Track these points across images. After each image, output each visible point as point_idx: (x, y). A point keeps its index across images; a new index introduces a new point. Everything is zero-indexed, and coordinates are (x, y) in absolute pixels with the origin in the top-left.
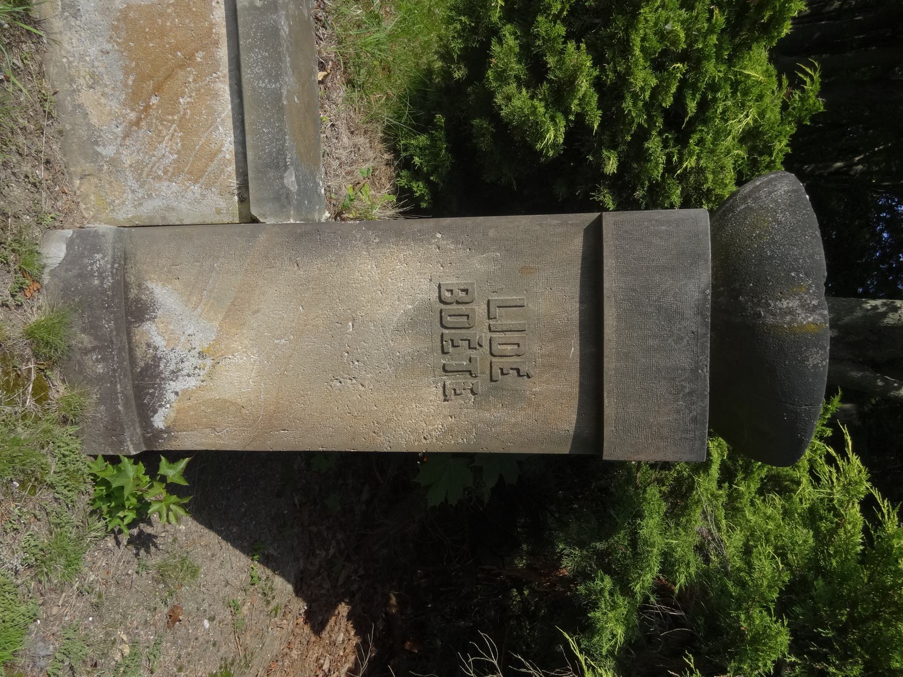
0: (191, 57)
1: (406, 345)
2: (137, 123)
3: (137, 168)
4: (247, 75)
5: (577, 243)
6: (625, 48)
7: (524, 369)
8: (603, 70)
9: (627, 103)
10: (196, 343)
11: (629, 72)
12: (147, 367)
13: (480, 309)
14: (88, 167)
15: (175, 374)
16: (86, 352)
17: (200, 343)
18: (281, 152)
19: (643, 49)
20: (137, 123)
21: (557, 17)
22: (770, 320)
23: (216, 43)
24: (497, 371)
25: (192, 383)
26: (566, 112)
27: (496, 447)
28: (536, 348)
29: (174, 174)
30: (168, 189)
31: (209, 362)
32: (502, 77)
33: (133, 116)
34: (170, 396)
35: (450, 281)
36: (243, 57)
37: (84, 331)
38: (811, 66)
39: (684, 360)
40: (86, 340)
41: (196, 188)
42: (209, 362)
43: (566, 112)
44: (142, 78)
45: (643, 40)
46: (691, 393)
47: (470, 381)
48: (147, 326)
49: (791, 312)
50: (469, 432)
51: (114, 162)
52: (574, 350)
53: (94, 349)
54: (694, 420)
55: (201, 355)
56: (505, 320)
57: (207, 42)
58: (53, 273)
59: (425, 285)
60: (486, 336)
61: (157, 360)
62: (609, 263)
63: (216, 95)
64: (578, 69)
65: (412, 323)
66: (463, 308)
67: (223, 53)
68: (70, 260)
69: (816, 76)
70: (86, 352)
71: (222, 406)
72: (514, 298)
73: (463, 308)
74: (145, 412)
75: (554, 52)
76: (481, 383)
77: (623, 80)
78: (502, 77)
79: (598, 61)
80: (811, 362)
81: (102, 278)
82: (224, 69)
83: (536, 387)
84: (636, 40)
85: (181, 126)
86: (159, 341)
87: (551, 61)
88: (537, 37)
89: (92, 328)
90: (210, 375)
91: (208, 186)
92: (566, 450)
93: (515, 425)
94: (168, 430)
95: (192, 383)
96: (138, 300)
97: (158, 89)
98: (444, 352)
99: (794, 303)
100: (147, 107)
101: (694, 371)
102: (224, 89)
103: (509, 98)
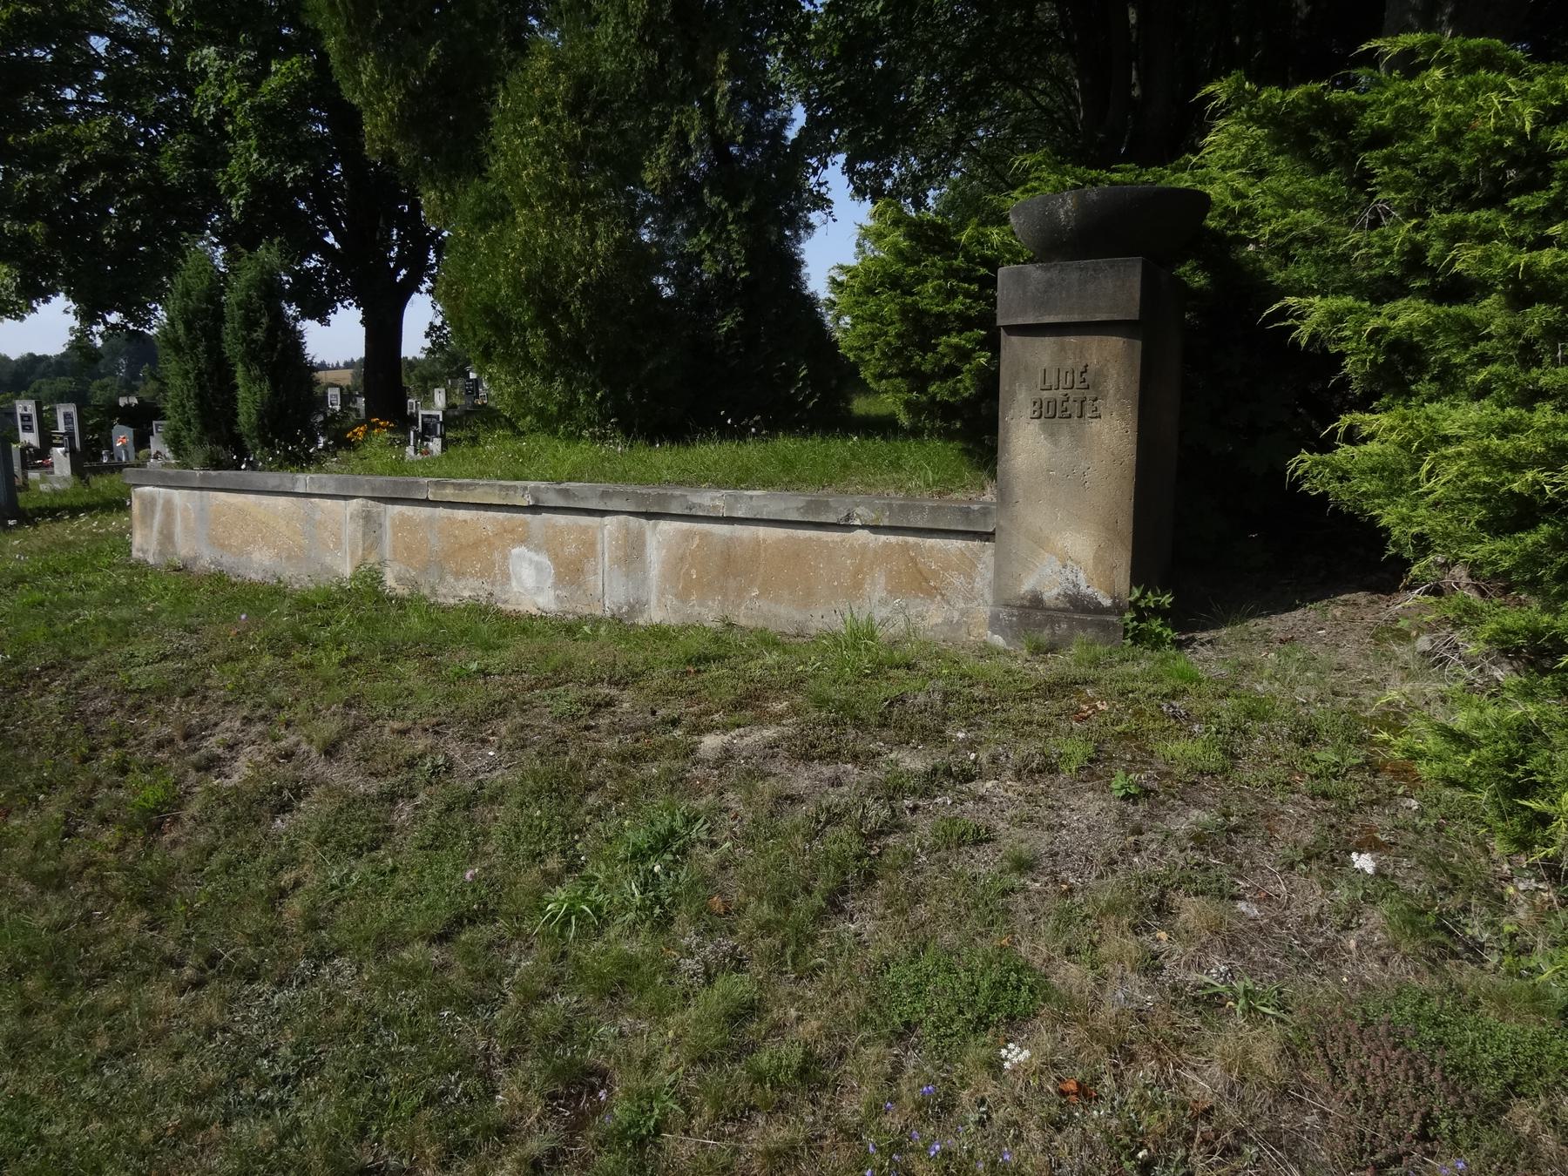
0: (912, 558)
1: (1065, 440)
2: (943, 595)
3: (966, 600)
4: (921, 525)
5: (1014, 339)
6: (942, 315)
7: (1081, 369)
8: (953, 329)
9: (973, 313)
10: (1057, 569)
11: (953, 313)
12: (1070, 602)
13: (1046, 394)
14: (964, 629)
15: (1076, 585)
16: (1054, 634)
17: (1057, 566)
18: (960, 509)
19: (945, 303)
20: (943, 595)
21: (923, 359)
22: (1073, 224)
23: (907, 543)
24: (1082, 385)
25: (1081, 575)
26: (973, 350)
27: (1136, 387)
28: (1070, 362)
29: (970, 577)
30: (979, 584)
31: (1069, 562)
32: (954, 392)
33: (939, 597)
34: (1089, 591)
35: (1029, 411)
36: (912, 525)
37: (1041, 632)
38: (1013, 163)
39: (1075, 276)
40: (1047, 632)
41: (980, 566)
42: (1069, 562)
43: (973, 350)
44: (921, 590)
45: (937, 305)
46: (1095, 270)
47: (1088, 402)
48: (1045, 597)
49: (1066, 213)
50: (1123, 404)
51: (963, 613)
52: (1072, 340)
53: (1052, 628)
54: (1111, 267)
55: (1065, 567)
56: (1052, 380)
57: (905, 548)
58: (1008, 644)
59: (1031, 427)
60: (1061, 391)
61: (1066, 595)
62: (1020, 321)
63: (932, 547)
64: (949, 346)
65: (1052, 435)
66: (1045, 405)
67: (911, 540)
68: (1002, 633)
69: (1021, 157)
70: (1054, 634)
71: (1098, 560)
72: (1040, 375)
73: (1045, 405)
74: (1099, 609)
75: (941, 360)
76: (1090, 394)
77: (960, 316)
78: (954, 392)
79: (947, 332)
80: (1095, 198)
81: (1013, 615)
82: (919, 540)
83: (1094, 361)
84: (936, 309)
85: (945, 570)
86: (1055, 591)
87: (946, 361)
88: (933, 370)
89: (1041, 626)
90: (1078, 563)
91: (979, 559)
92: (1138, 344)
93: (1119, 374)
94: (1114, 598)
95: (1081, 575)
96: (1030, 601)
97: (927, 581)
98: (1070, 416)
99: (1061, 211)
100: (935, 588)
101: (1081, 269)
102: (930, 542)
103: (966, 389)
